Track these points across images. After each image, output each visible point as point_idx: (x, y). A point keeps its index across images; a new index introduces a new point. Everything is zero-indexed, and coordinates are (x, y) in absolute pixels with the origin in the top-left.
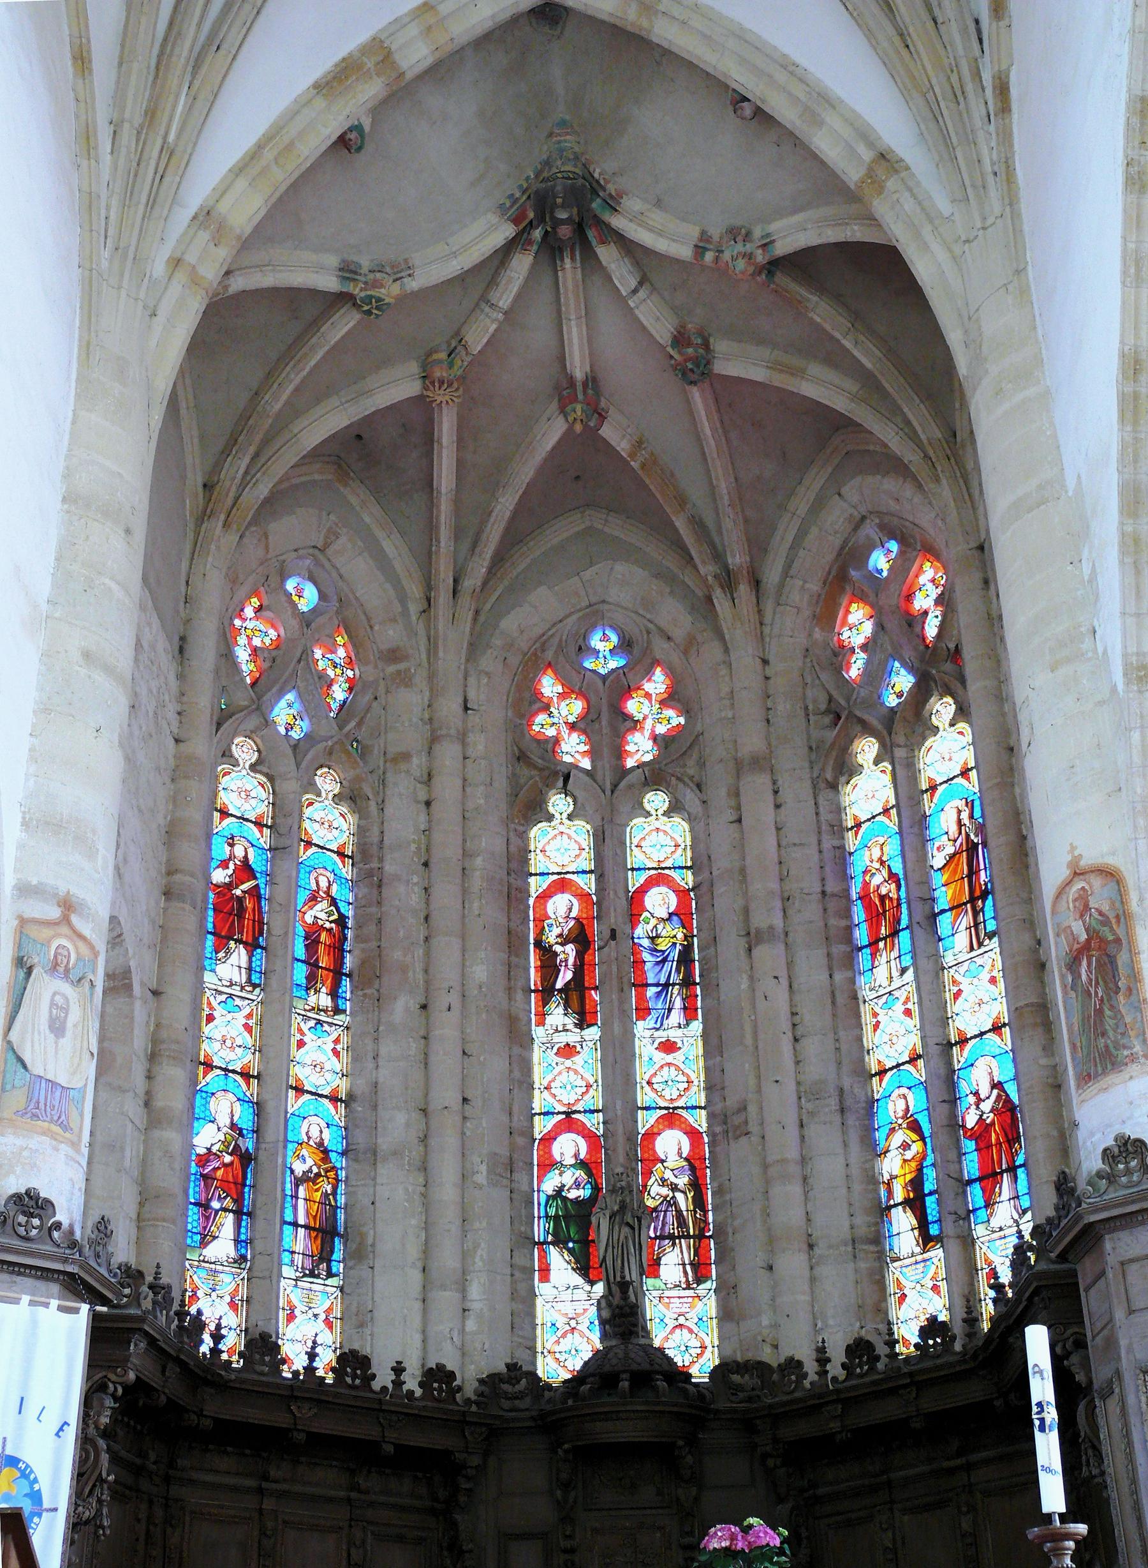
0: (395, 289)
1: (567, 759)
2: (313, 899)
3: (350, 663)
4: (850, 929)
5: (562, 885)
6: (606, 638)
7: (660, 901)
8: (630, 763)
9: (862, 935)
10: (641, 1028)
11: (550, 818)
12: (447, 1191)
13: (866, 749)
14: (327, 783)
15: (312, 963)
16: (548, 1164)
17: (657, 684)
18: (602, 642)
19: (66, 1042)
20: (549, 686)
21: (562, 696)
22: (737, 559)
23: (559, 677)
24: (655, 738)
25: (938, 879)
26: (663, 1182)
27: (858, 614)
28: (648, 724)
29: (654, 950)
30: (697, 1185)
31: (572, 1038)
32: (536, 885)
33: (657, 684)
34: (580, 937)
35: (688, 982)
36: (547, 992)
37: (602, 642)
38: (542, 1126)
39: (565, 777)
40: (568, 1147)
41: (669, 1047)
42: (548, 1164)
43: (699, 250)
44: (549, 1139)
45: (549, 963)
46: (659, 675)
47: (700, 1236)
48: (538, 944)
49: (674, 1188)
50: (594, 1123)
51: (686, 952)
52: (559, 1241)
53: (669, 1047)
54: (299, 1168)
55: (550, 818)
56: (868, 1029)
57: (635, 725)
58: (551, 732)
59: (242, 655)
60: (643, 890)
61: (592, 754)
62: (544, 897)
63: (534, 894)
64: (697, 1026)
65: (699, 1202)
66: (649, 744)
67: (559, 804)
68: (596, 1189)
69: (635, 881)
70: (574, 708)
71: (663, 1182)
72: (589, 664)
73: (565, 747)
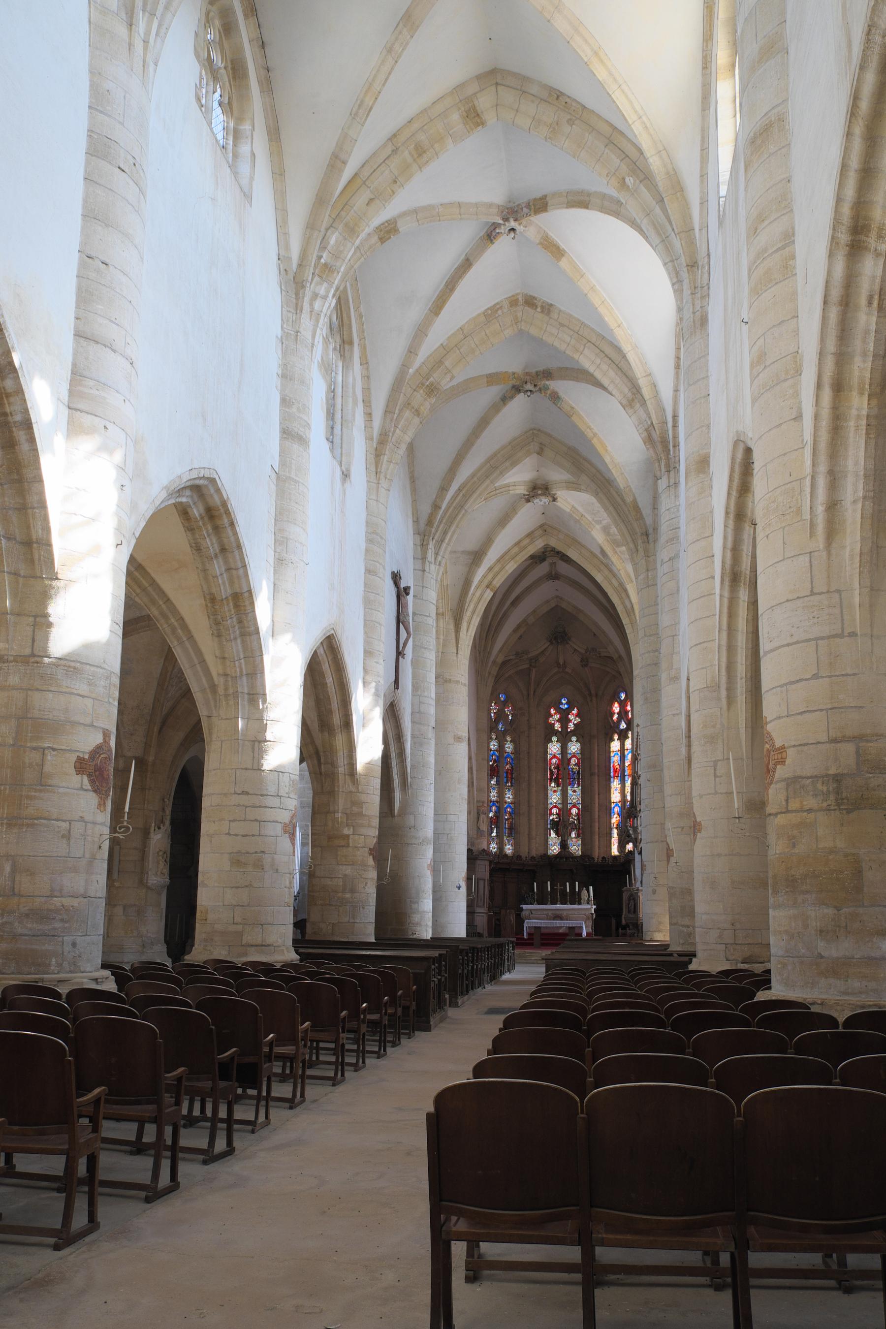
0: (526, 657)
1: (556, 728)
2: (507, 764)
3: (512, 710)
4: (610, 773)
5: (554, 757)
6: (565, 700)
7: (574, 761)
8: (569, 730)
9: (612, 774)
10: (569, 788)
11: (552, 742)
12: (533, 822)
13: (616, 737)
14: (509, 739)
15: (507, 777)
16: (551, 814)
17: (575, 712)
19: (485, 824)
20: (553, 711)
21: (555, 714)
22: (593, 692)
23: (555, 709)
24: (574, 724)
25: (626, 769)
26: (573, 818)
27: (616, 705)
28: (573, 721)
29: (572, 771)
30: (578, 819)
31: (556, 789)
32: (549, 757)
33: (575, 712)
34: (557, 768)
35: (579, 779)
36: (551, 780)
38: (550, 806)
39: (556, 733)
40: (554, 811)
41: (574, 791)
42: (551, 814)
43: (586, 652)
44: (551, 809)
45: (552, 773)
46: (576, 709)
47: (579, 829)
48: (550, 769)
49: (574, 819)
50: (560, 806)
51: (579, 771)
52: (553, 829)
53: (574, 791)
54: (506, 817)
55: (552, 742)
56: (612, 794)
57: (570, 721)
58: (553, 722)
59: (492, 715)
60: (570, 758)
61: (561, 727)
62: (551, 759)
63: (549, 758)
64: (580, 787)
65: (579, 822)
66: (573, 726)
67: (554, 739)
68: (560, 819)
69: (569, 756)
70: (557, 717)
71: (573, 818)
72: (561, 706)
73: (556, 726)
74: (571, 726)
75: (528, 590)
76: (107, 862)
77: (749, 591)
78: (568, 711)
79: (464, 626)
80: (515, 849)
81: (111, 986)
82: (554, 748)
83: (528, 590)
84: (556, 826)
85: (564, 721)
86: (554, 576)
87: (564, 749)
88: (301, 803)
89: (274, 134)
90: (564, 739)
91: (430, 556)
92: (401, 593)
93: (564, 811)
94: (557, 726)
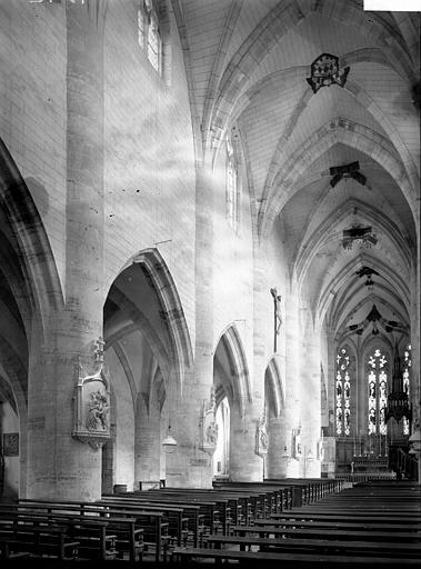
7: (383, 384)
18: (377, 351)
37: (377, 351)
74: (382, 365)
76: (302, 477)
78: (344, 371)
79: (318, 315)
81: (226, 401)
82: (372, 377)
84: (373, 419)
85: (377, 362)
86: (369, 283)
87: (377, 379)
88: (93, 529)
89: (183, 36)
90: (377, 371)
91: (295, 275)
92: (277, 299)
94: (374, 366)
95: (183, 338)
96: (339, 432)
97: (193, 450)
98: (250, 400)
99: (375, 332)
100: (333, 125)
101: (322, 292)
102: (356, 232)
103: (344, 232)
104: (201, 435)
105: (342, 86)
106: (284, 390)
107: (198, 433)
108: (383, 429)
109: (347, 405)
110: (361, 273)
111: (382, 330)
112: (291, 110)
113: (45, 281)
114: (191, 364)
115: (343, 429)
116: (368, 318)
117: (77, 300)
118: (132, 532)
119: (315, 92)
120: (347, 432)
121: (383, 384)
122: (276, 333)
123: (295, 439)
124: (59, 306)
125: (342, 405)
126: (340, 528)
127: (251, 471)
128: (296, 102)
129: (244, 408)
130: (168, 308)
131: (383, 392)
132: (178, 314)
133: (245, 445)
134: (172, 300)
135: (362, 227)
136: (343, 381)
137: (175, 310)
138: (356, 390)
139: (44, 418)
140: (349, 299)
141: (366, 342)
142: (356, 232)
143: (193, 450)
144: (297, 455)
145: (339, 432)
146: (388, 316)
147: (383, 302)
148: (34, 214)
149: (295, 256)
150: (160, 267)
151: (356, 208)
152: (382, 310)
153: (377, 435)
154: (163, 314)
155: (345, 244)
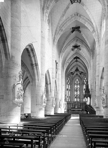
7: (78, 88)
74: (78, 83)
75: (72, 63)
77: (32, 101)
79: (64, 69)
80: (80, 100)
82: (76, 86)
83: (72, 63)
85: (77, 82)
87: (77, 87)
90: (77, 84)
92: (57, 63)
93: (77, 96)
95: (37, 72)
96: (67, 100)
97: (40, 106)
98: (51, 91)
99: (77, 74)
100: (75, 15)
101: (66, 62)
102: (76, 47)
103: (73, 46)
104: (42, 101)
105: (80, 3)
106: (57, 89)
107: (41, 101)
108: (78, 100)
109: (69, 93)
110: (75, 58)
111: (79, 74)
112: (65, 9)
113: (5, 47)
114: (39, 80)
115: (68, 100)
116: (75, 70)
117: (14, 57)
118: (48, 131)
119: (72, 4)
120: (69, 101)
121: (78, 88)
122: (56, 73)
123: (60, 102)
124: (9, 58)
125: (69, 93)
126: (31, 124)
127: (50, 111)
128: (66, 6)
129: (49, 94)
130: (34, 63)
131: (78, 90)
132: (36, 65)
133: (50, 104)
134: (35, 61)
135: (77, 45)
136: (68, 87)
137: (36, 64)
138: (72, 90)
139: (3, 96)
140: (71, 65)
141: (75, 76)
142: (76, 47)
143: (40, 106)
144: (61, 107)
145: (67, 100)
146: (80, 70)
147: (80, 66)
148: (2, 26)
149: (60, 52)
150: (33, 50)
151: (77, 40)
152: (79, 69)
153: (77, 102)
154: (32, 65)
155: (73, 50)
